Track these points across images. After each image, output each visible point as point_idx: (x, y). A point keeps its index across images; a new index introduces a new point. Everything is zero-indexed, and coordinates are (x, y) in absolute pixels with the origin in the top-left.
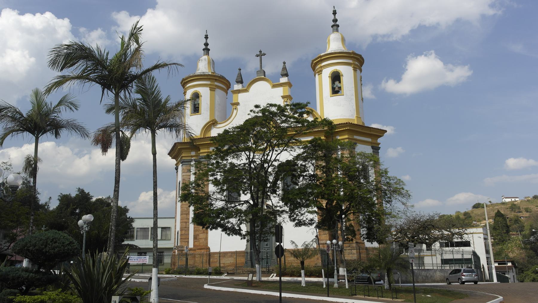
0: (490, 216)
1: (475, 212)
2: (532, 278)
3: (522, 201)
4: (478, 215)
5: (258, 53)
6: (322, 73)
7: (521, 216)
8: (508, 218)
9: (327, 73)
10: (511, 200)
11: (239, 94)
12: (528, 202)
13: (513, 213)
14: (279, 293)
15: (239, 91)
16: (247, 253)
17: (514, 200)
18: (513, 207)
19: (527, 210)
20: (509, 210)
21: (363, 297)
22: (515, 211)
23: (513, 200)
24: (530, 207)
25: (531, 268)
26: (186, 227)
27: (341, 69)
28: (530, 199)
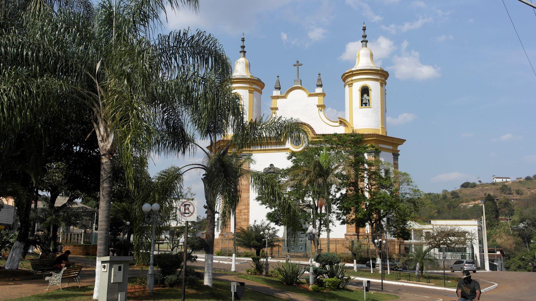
0: (479, 196)
1: (463, 192)
2: (518, 265)
3: (513, 182)
4: (467, 195)
5: (296, 63)
6: (352, 86)
7: (512, 198)
8: (497, 200)
9: (357, 86)
10: (502, 180)
11: (278, 100)
12: (519, 184)
13: (503, 195)
14: (109, 260)
15: (278, 97)
17: (505, 181)
18: (504, 188)
19: (518, 192)
20: (499, 191)
21: (426, 283)
22: (505, 192)
23: (504, 180)
24: (521, 189)
25: (518, 255)
27: (370, 84)
28: (522, 180)
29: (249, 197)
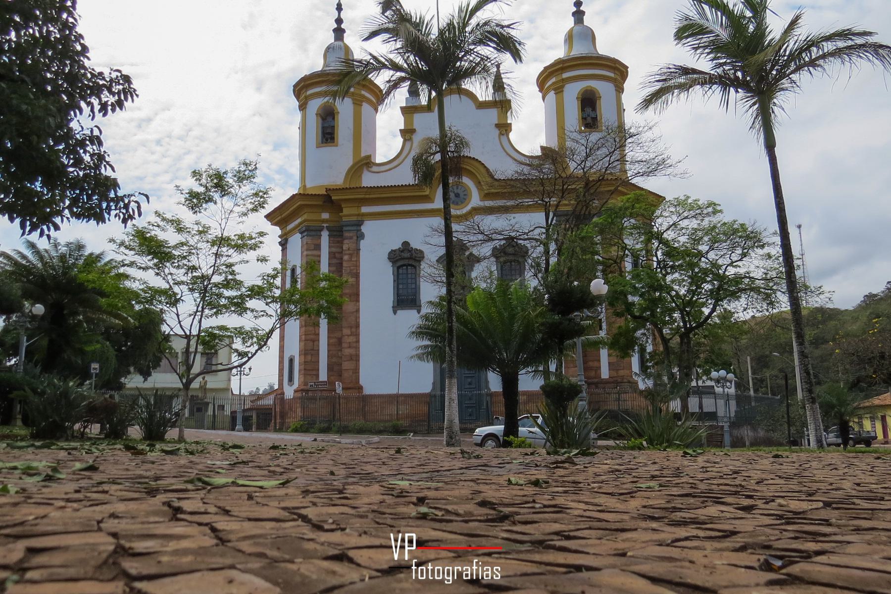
6: (563, 91)
16: (435, 396)
26: (313, 350)
29: (358, 311)
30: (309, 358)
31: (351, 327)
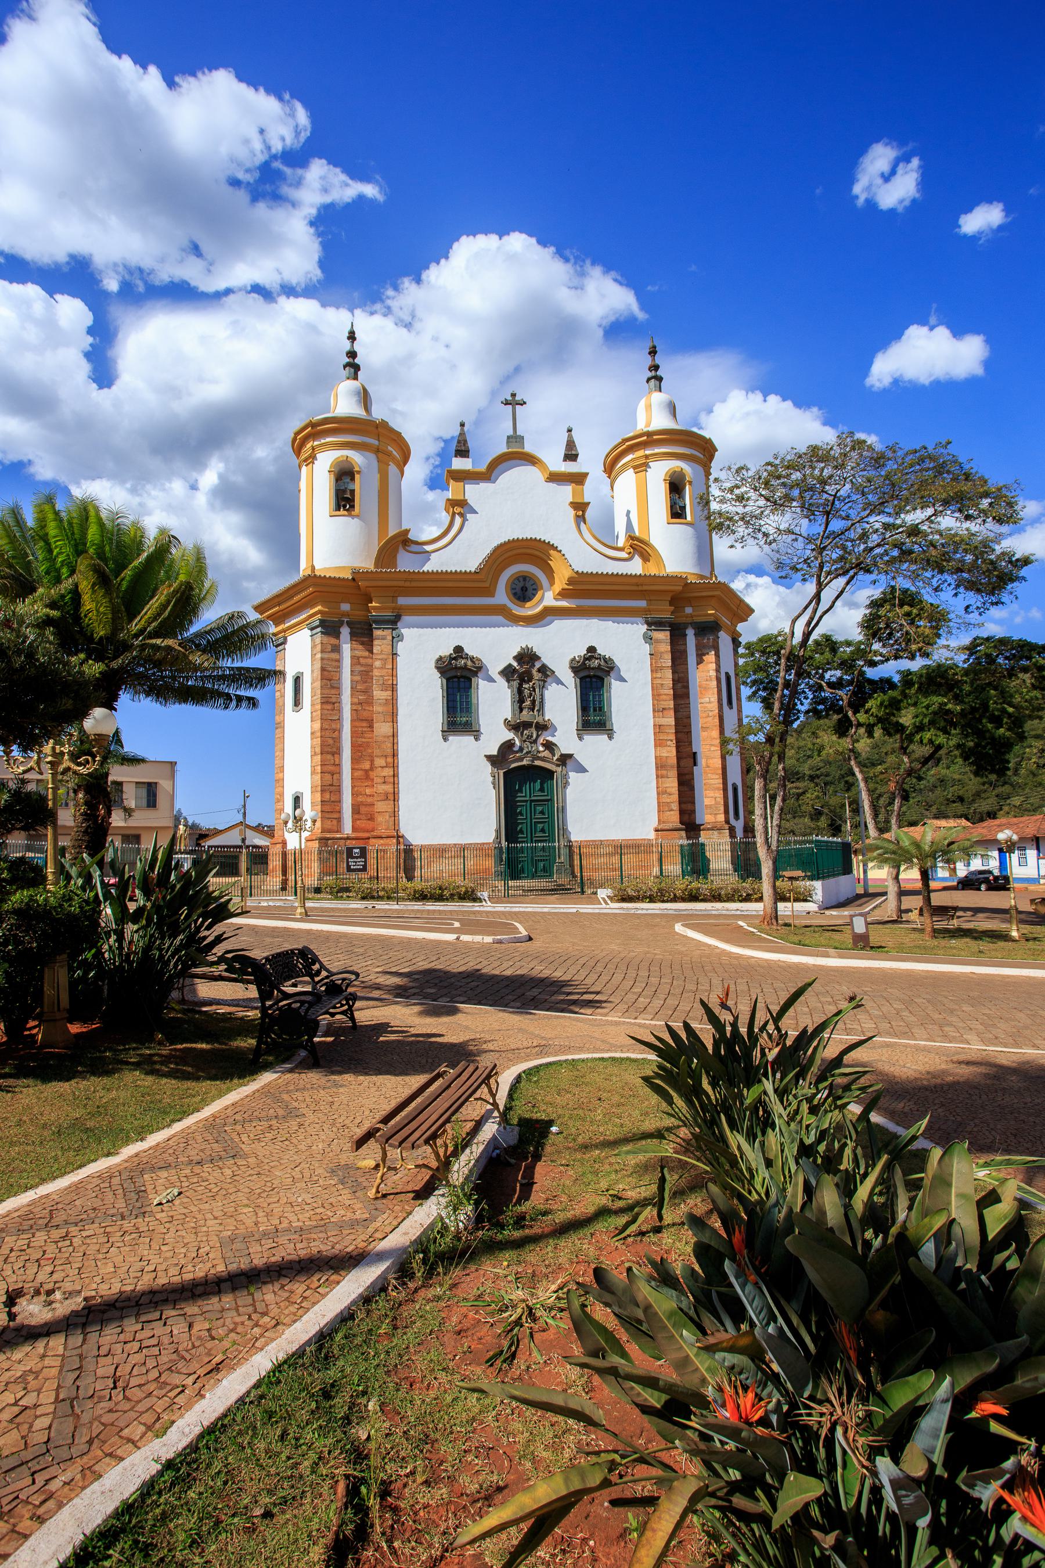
9: (326, 461)
26: (332, 785)
27: (357, 458)
30: (327, 796)
31: (386, 756)
